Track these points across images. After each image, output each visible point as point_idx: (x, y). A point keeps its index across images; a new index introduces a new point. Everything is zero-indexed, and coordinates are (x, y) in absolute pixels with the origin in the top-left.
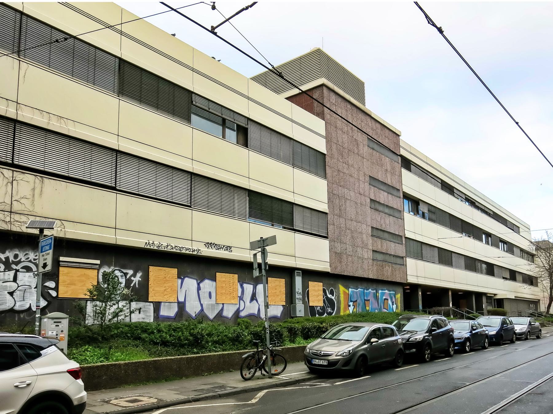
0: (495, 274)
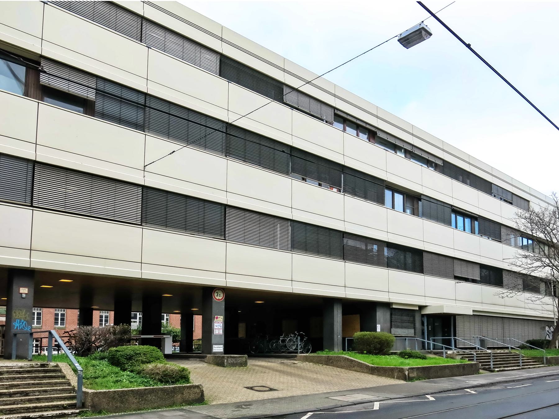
0: (425, 269)
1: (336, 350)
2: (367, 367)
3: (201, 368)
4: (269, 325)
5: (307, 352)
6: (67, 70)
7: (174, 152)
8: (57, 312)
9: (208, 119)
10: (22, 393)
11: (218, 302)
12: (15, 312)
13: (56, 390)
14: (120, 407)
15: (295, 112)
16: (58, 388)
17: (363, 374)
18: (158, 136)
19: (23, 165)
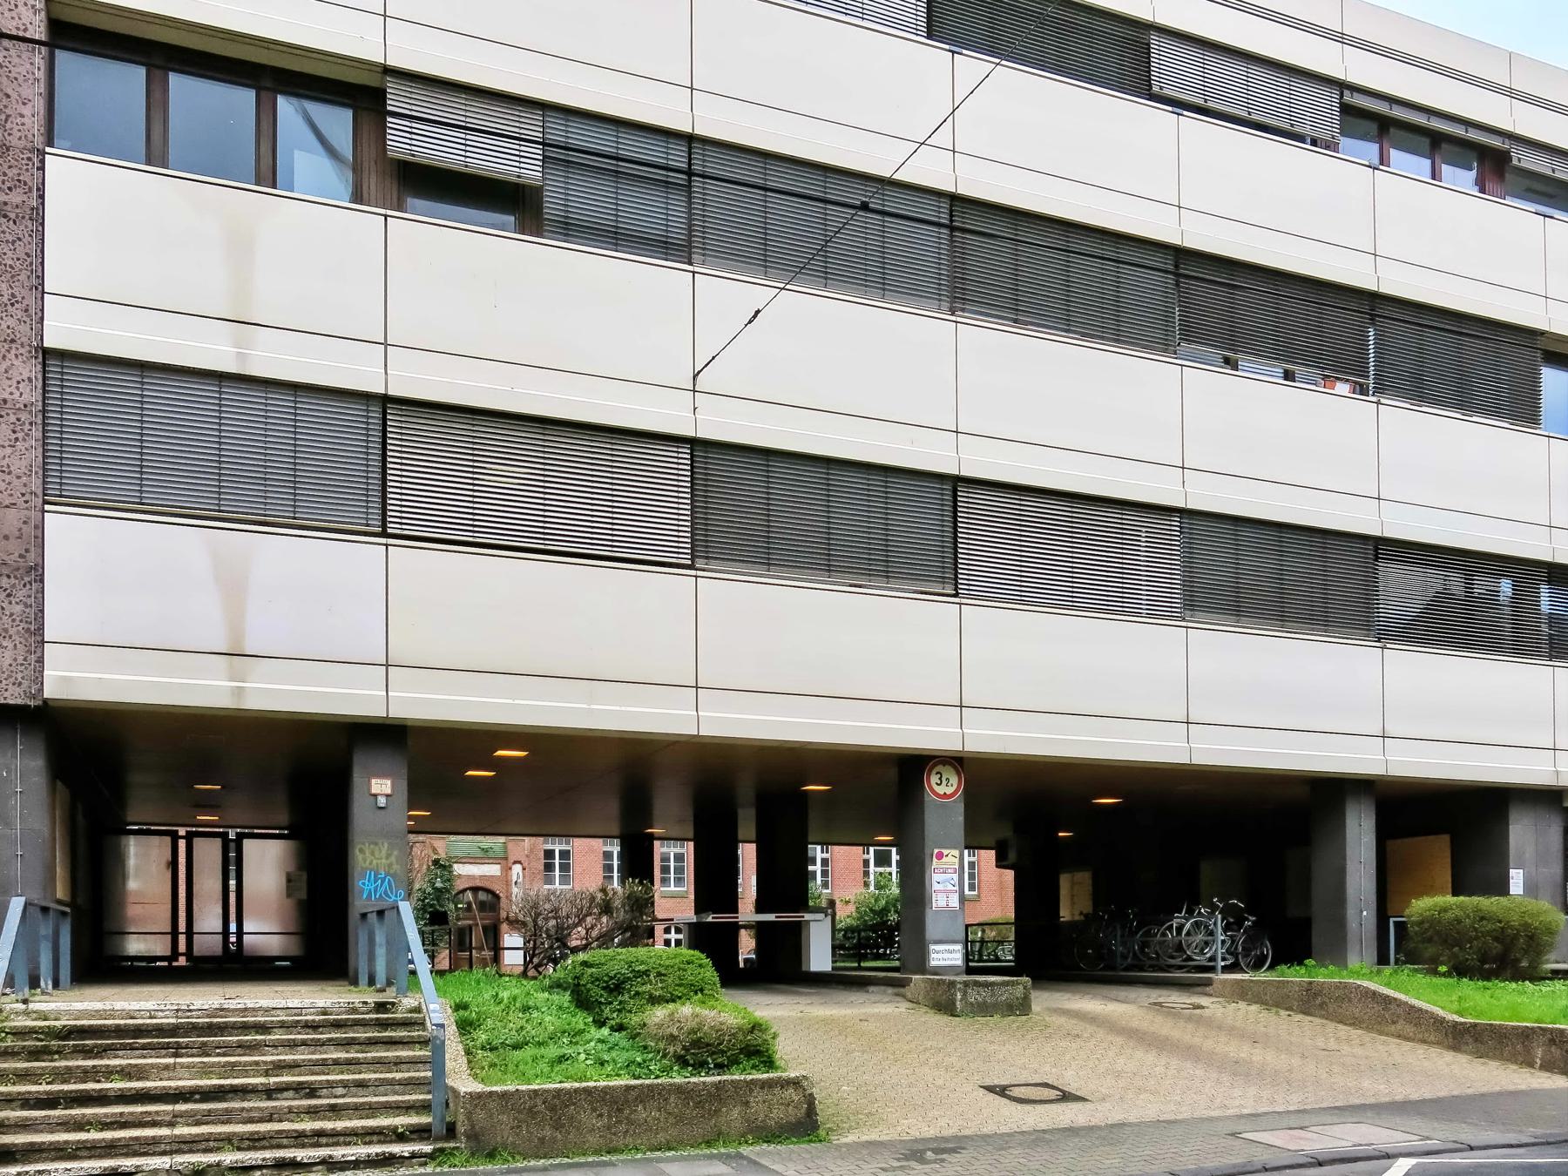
1: (1354, 962)
2: (1439, 1022)
3: (878, 1017)
4: (1143, 875)
5: (1257, 965)
6: (460, 100)
7: (758, 312)
8: (549, 847)
9: (772, 165)
10: (298, 1088)
11: (943, 805)
12: (361, 851)
13: (391, 1082)
14: (554, 1140)
15: (1190, 122)
16: (398, 1076)
17: (1421, 1050)
18: (735, 271)
19: (355, 410)
